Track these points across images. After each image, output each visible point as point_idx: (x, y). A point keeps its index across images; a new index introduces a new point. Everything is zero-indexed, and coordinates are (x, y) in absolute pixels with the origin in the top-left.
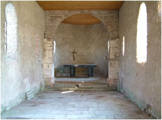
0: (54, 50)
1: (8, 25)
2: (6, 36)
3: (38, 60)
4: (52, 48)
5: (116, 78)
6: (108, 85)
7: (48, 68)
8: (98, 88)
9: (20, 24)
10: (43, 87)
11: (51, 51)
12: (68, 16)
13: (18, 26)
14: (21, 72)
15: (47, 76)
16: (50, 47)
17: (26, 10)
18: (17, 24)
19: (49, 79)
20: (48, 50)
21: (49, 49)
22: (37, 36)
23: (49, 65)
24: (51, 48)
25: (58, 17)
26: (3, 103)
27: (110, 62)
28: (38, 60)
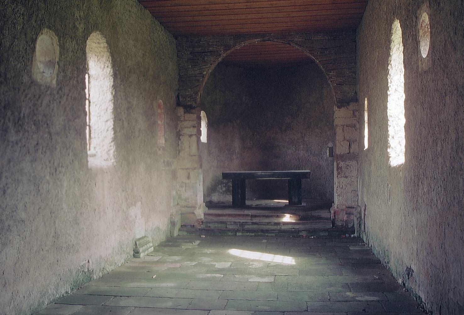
0: (201, 135)
1: (91, 79)
2: (89, 106)
3: (164, 162)
4: (195, 130)
5: (353, 204)
6: (333, 223)
7: (187, 181)
8: (230, 215)
9: (119, 77)
10: (178, 227)
11: (194, 138)
12: (232, 50)
13: (114, 81)
14: (123, 191)
15: (186, 200)
16: (192, 129)
17: (132, 42)
18: (111, 77)
19: (191, 207)
20: (188, 136)
21: (190, 133)
22: (161, 101)
23: (189, 174)
24: (194, 131)
25: (209, 54)
26: (84, 262)
27: (338, 165)
28: (162, 161)
